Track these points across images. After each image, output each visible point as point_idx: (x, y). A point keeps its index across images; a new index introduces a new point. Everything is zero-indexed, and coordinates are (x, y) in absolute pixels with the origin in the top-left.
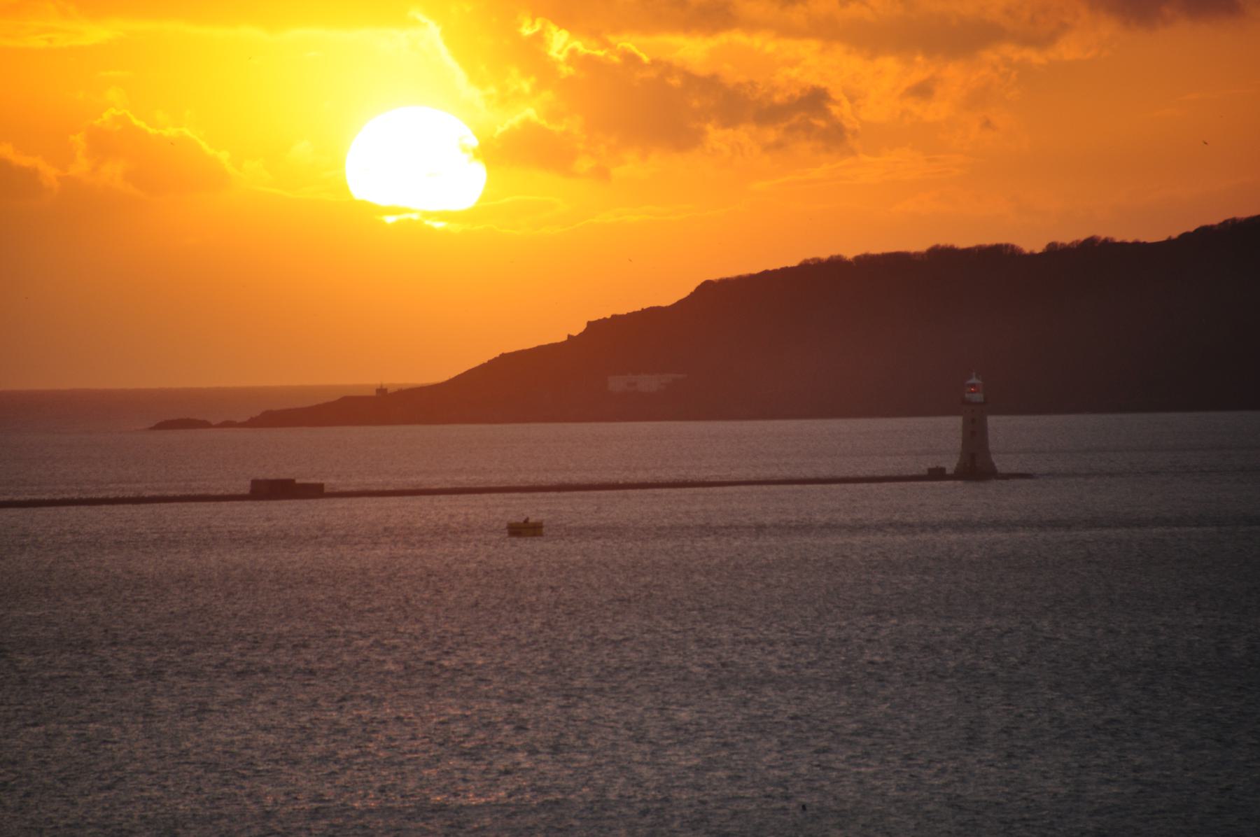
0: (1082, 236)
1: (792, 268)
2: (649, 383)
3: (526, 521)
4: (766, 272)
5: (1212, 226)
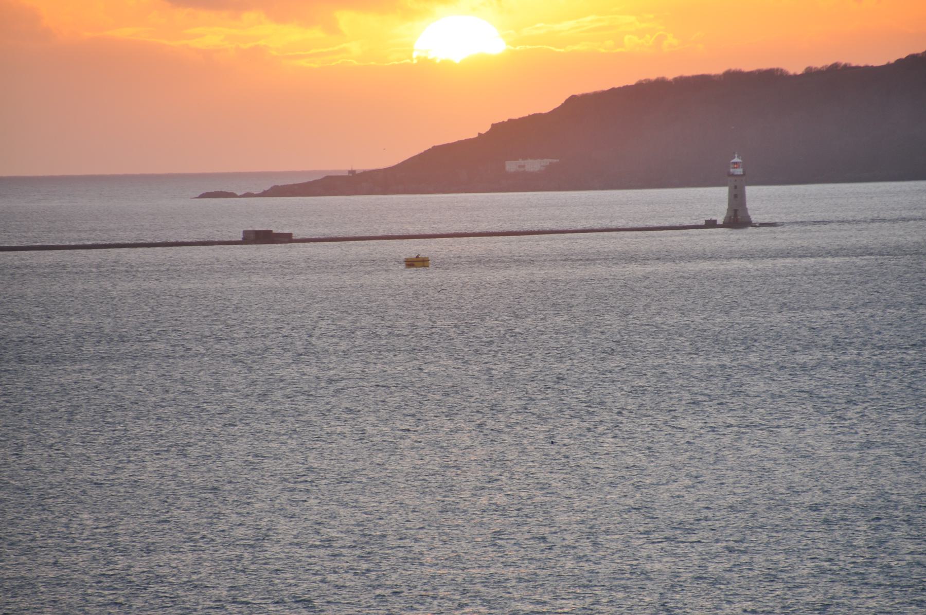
2: (534, 165)
3: (417, 257)
4: (613, 89)
5: (918, 54)
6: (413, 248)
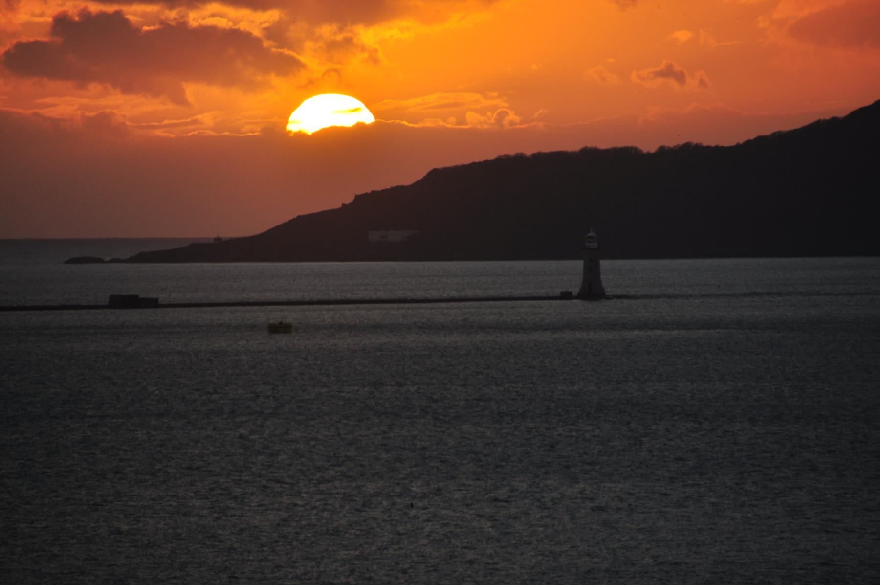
0: (681, 142)
1: (491, 161)
3: (281, 323)
4: (474, 163)
5: (766, 136)
6: (275, 315)
